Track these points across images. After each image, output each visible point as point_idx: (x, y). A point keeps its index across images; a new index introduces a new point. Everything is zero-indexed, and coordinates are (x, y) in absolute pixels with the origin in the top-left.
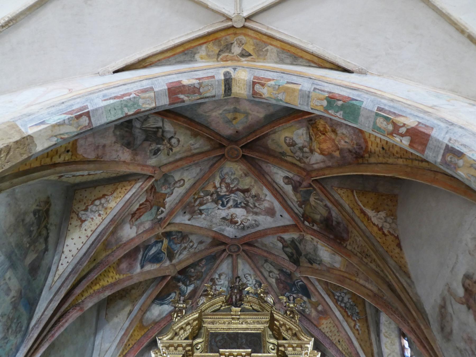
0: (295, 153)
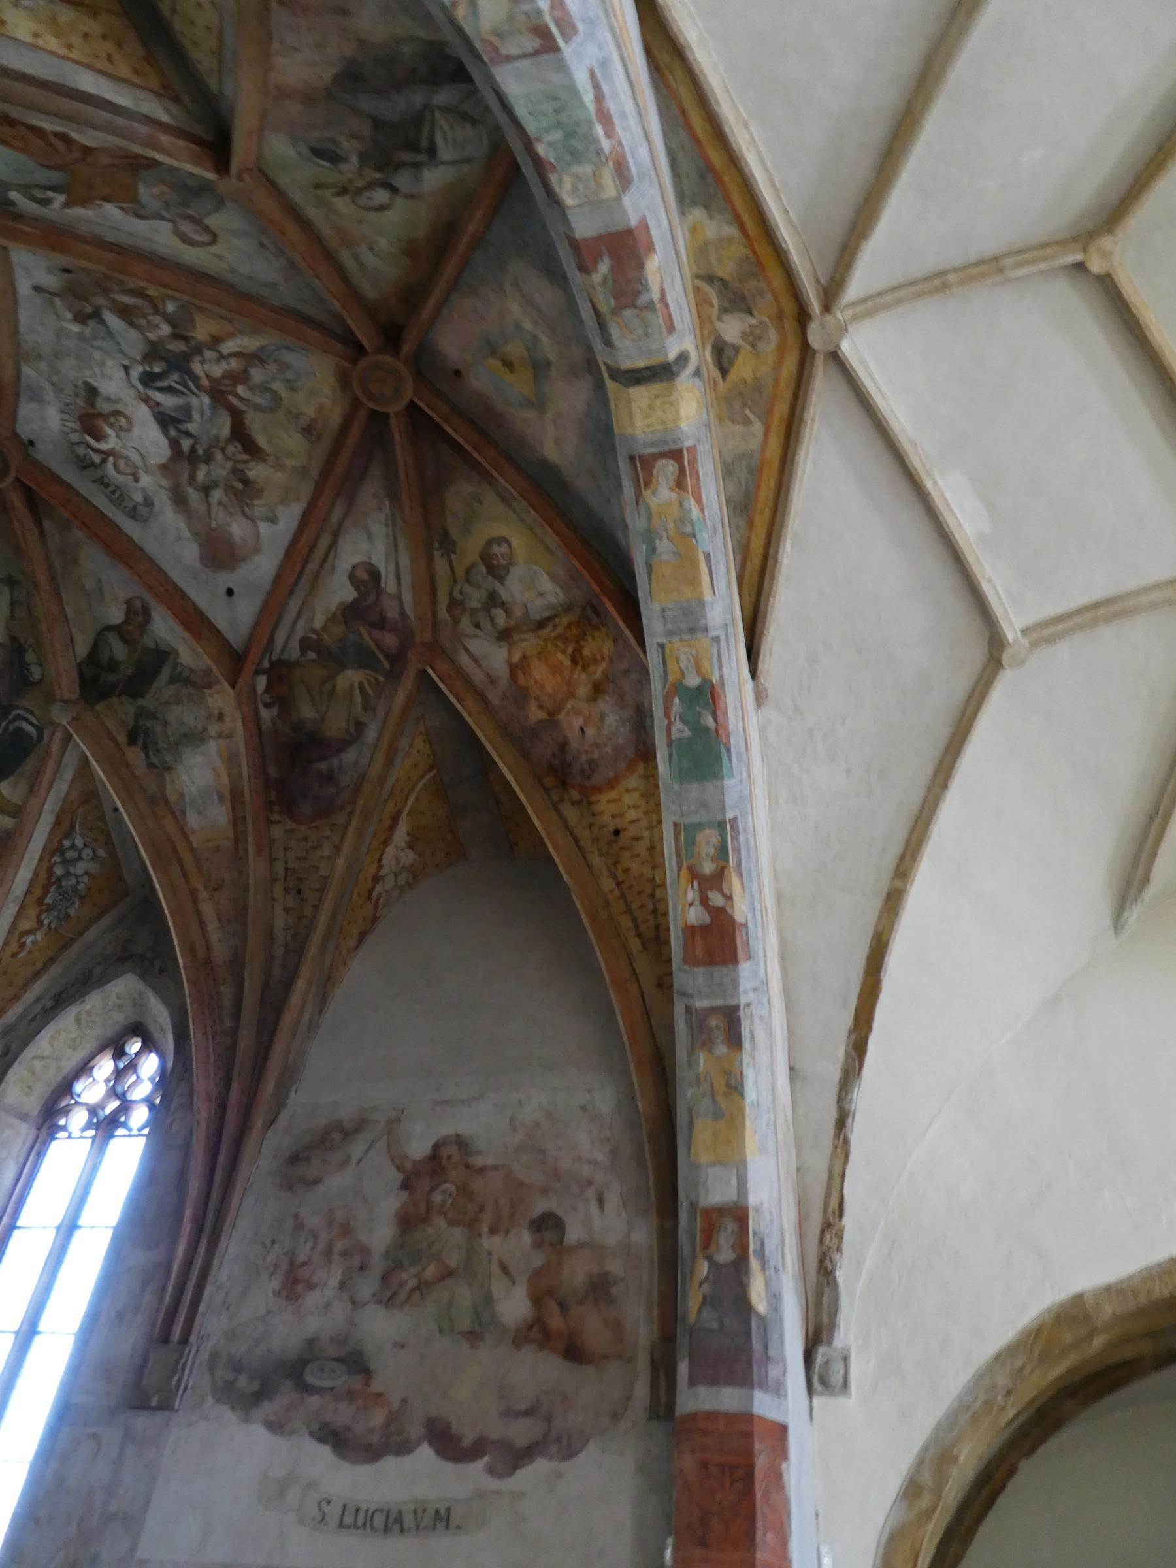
0: (468, 581)
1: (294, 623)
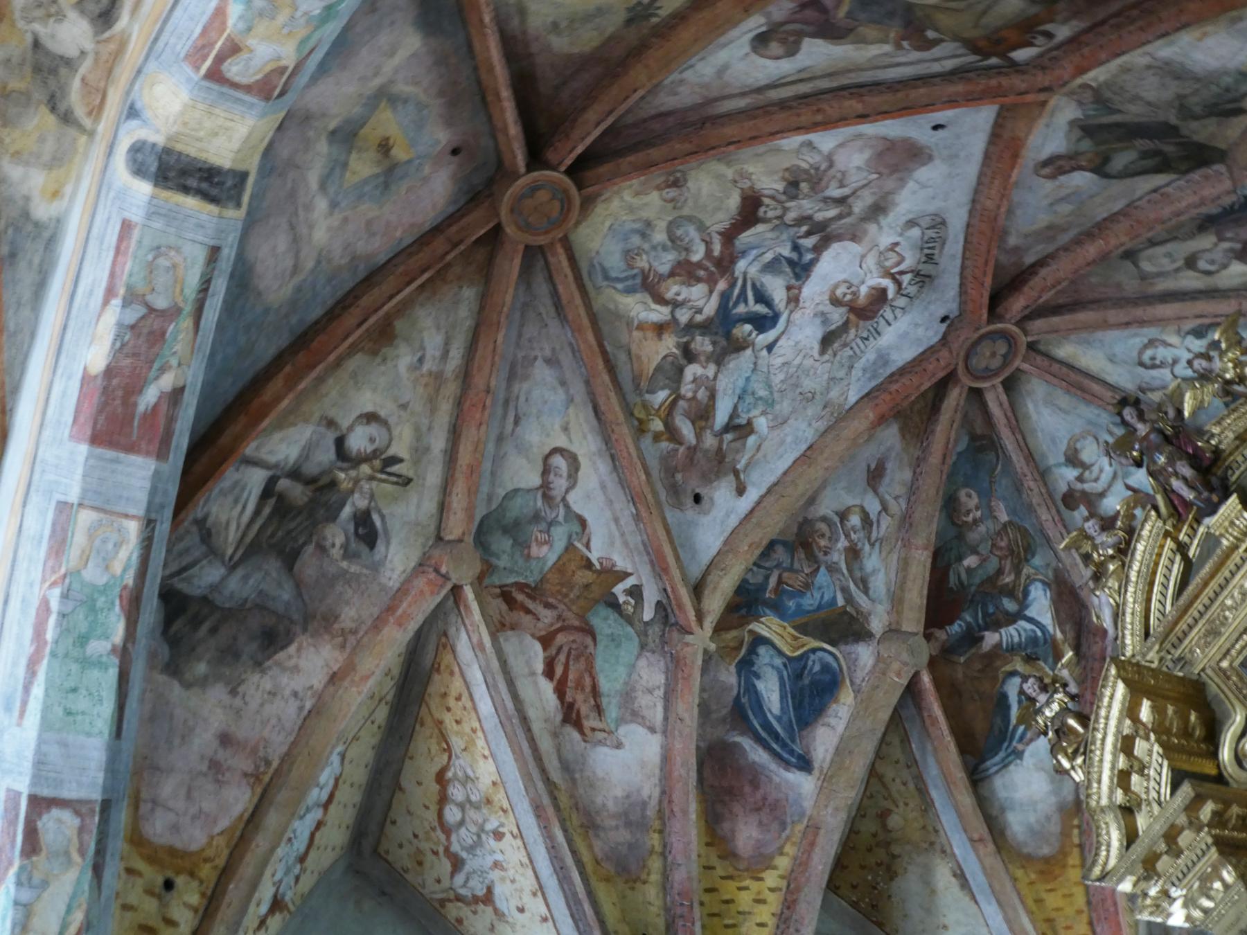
1: (911, 63)
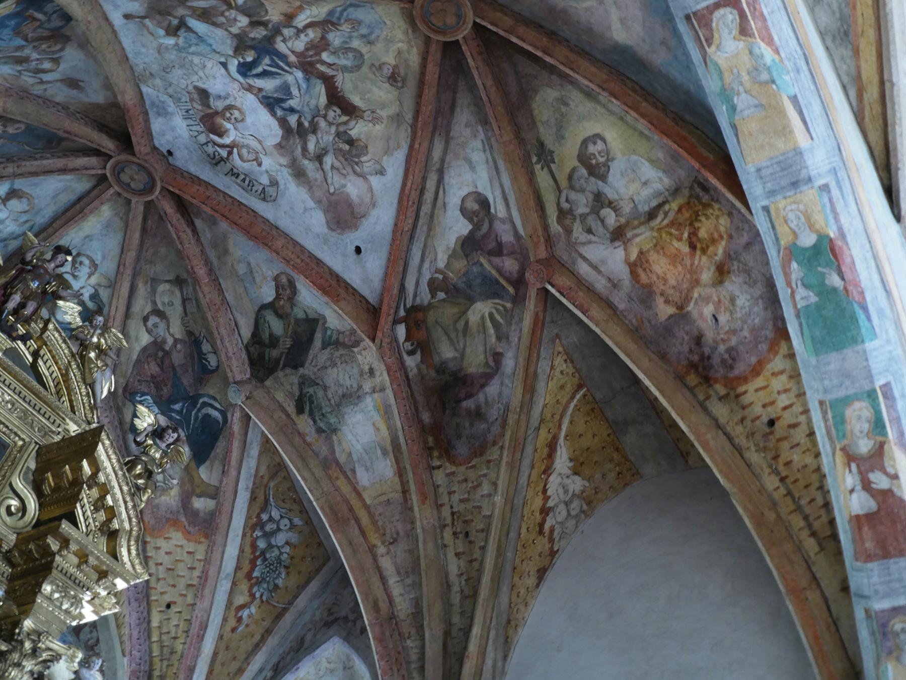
0: (571, 187)
